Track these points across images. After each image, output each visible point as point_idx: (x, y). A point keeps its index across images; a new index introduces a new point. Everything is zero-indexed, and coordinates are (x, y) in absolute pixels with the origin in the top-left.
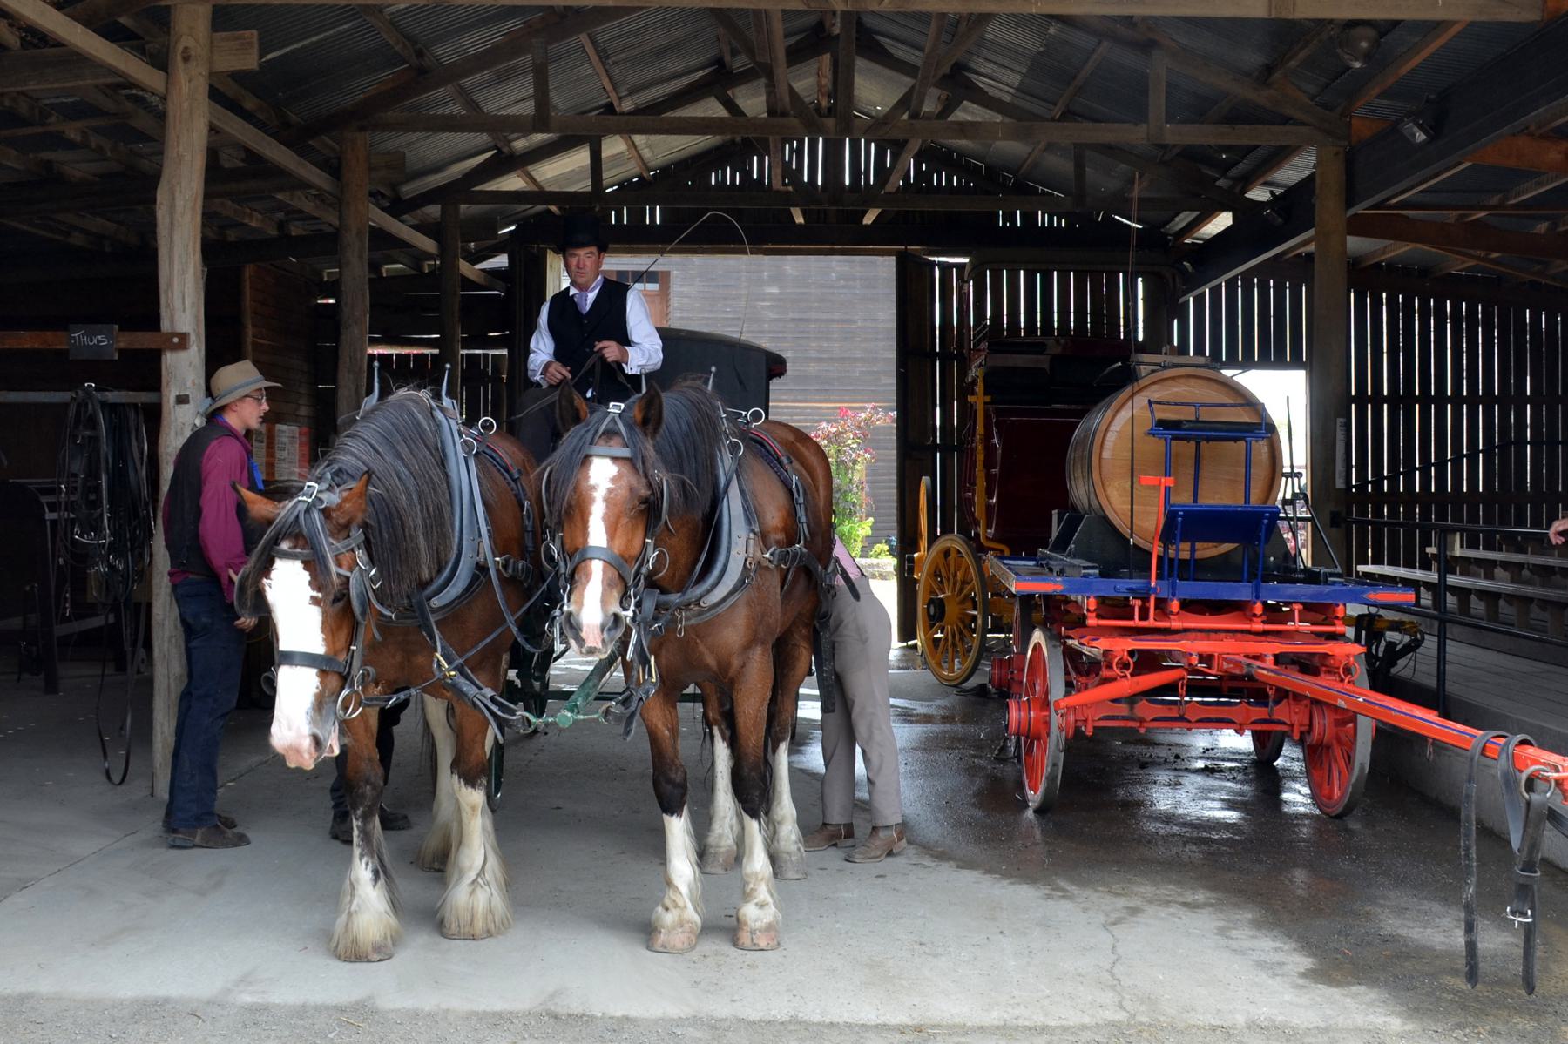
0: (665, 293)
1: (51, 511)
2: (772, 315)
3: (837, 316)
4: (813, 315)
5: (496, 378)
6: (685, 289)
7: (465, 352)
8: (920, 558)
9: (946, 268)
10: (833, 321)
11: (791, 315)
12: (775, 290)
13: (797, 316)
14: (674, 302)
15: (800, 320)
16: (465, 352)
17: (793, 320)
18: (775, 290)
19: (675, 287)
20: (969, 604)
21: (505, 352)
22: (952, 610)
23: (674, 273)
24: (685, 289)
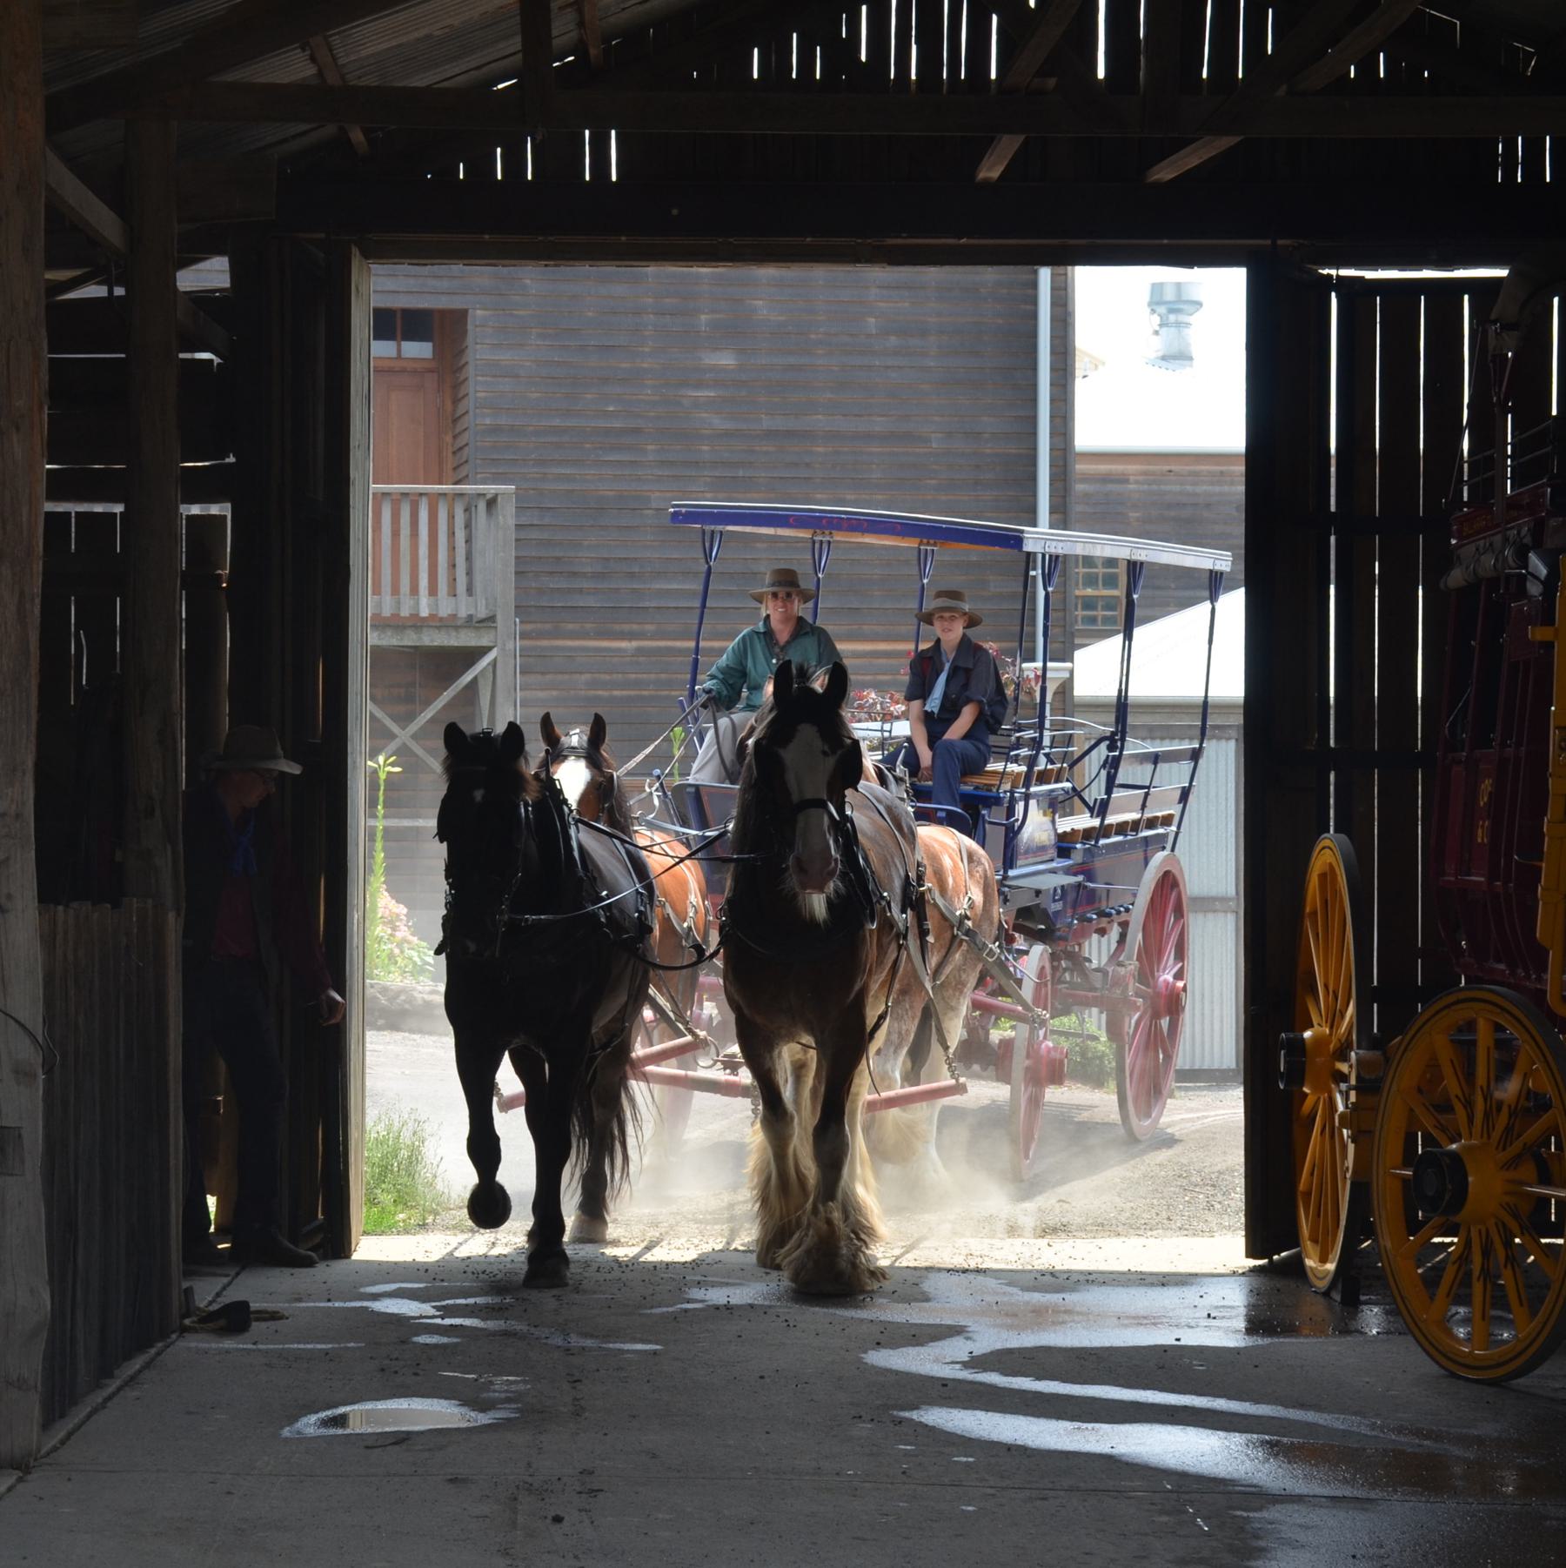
0: (449, 366)
1: (734, 1056)
2: (719, 423)
3: (879, 425)
4: (819, 421)
5: (199, 579)
6: (505, 357)
7: (195, 510)
8: (1319, 1041)
9: (1355, 293)
10: (869, 437)
11: (767, 423)
12: (726, 360)
13: (780, 423)
14: (478, 386)
15: (790, 434)
16: (195, 510)
17: (770, 434)
18: (726, 360)
19: (480, 350)
20: (1528, 1170)
21: (118, 509)
22: (1485, 1185)
23: (478, 314)
24: (505, 357)
